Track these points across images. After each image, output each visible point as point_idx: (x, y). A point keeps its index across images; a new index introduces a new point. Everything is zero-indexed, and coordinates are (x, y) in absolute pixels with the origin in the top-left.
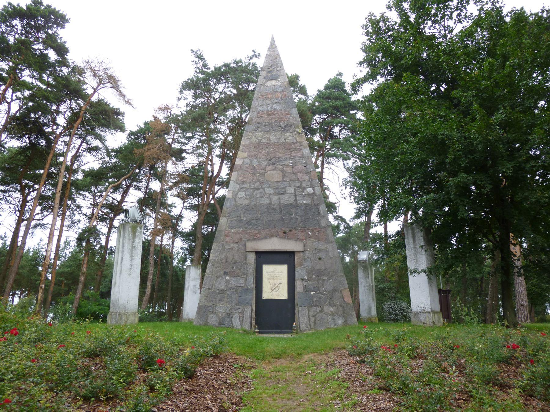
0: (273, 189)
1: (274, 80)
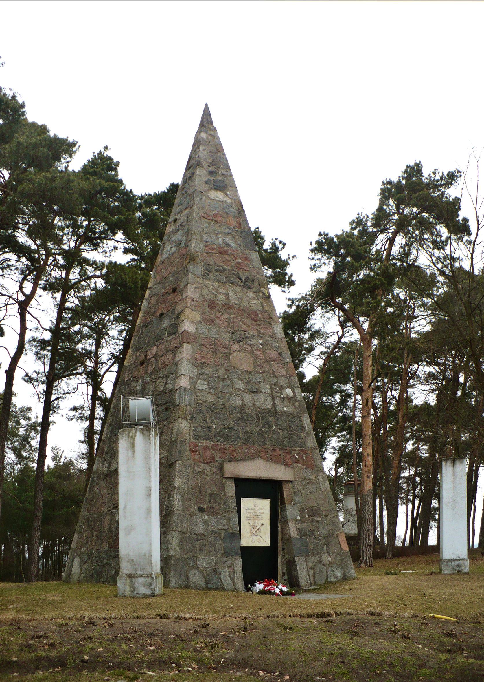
0: (244, 382)
1: (220, 190)
